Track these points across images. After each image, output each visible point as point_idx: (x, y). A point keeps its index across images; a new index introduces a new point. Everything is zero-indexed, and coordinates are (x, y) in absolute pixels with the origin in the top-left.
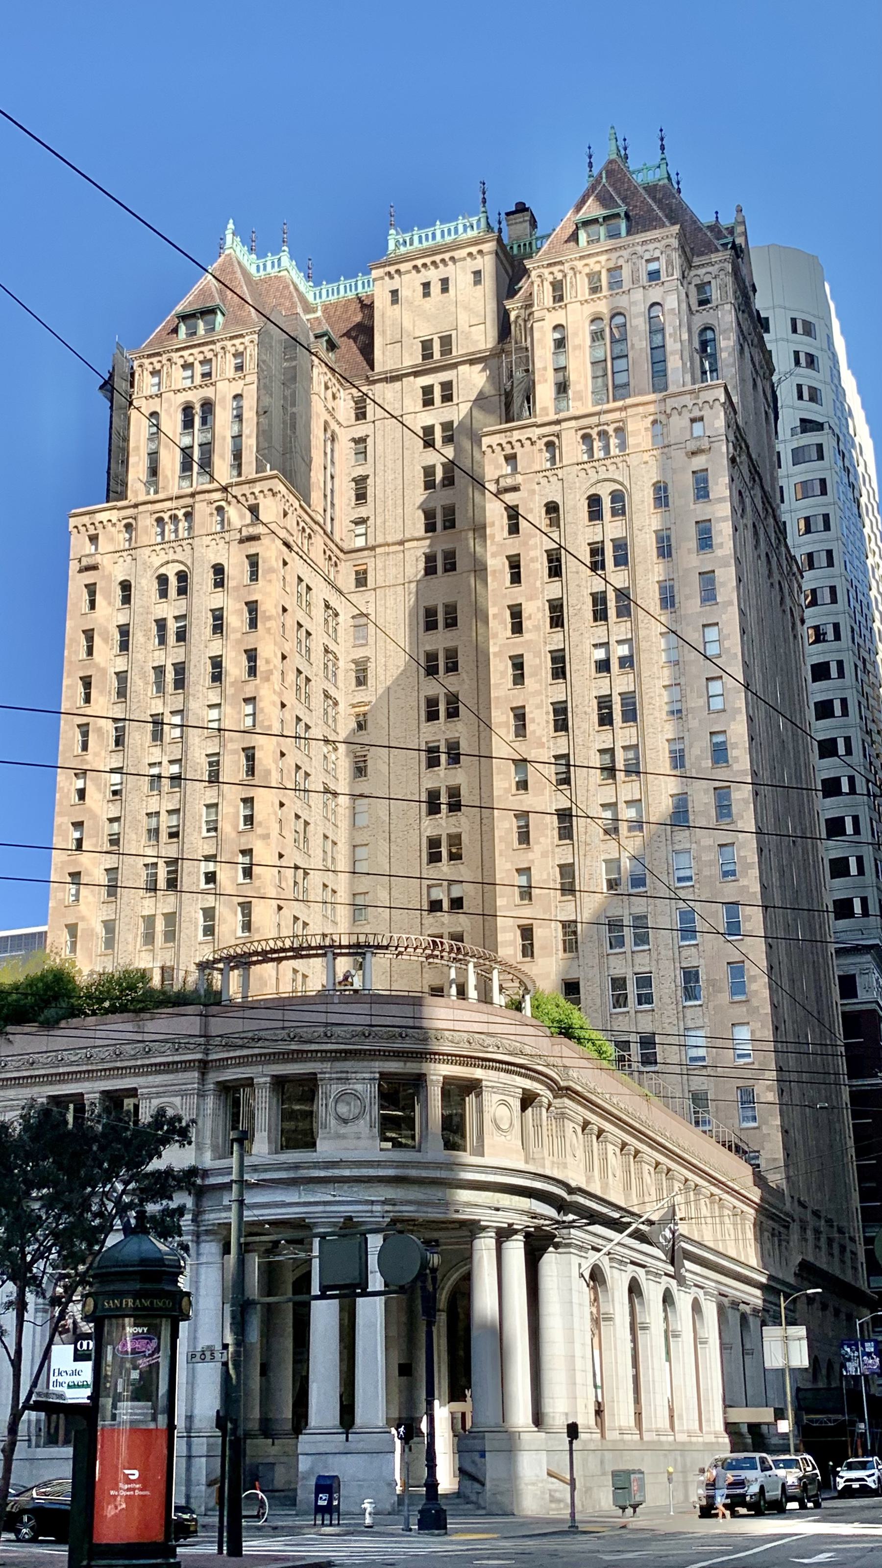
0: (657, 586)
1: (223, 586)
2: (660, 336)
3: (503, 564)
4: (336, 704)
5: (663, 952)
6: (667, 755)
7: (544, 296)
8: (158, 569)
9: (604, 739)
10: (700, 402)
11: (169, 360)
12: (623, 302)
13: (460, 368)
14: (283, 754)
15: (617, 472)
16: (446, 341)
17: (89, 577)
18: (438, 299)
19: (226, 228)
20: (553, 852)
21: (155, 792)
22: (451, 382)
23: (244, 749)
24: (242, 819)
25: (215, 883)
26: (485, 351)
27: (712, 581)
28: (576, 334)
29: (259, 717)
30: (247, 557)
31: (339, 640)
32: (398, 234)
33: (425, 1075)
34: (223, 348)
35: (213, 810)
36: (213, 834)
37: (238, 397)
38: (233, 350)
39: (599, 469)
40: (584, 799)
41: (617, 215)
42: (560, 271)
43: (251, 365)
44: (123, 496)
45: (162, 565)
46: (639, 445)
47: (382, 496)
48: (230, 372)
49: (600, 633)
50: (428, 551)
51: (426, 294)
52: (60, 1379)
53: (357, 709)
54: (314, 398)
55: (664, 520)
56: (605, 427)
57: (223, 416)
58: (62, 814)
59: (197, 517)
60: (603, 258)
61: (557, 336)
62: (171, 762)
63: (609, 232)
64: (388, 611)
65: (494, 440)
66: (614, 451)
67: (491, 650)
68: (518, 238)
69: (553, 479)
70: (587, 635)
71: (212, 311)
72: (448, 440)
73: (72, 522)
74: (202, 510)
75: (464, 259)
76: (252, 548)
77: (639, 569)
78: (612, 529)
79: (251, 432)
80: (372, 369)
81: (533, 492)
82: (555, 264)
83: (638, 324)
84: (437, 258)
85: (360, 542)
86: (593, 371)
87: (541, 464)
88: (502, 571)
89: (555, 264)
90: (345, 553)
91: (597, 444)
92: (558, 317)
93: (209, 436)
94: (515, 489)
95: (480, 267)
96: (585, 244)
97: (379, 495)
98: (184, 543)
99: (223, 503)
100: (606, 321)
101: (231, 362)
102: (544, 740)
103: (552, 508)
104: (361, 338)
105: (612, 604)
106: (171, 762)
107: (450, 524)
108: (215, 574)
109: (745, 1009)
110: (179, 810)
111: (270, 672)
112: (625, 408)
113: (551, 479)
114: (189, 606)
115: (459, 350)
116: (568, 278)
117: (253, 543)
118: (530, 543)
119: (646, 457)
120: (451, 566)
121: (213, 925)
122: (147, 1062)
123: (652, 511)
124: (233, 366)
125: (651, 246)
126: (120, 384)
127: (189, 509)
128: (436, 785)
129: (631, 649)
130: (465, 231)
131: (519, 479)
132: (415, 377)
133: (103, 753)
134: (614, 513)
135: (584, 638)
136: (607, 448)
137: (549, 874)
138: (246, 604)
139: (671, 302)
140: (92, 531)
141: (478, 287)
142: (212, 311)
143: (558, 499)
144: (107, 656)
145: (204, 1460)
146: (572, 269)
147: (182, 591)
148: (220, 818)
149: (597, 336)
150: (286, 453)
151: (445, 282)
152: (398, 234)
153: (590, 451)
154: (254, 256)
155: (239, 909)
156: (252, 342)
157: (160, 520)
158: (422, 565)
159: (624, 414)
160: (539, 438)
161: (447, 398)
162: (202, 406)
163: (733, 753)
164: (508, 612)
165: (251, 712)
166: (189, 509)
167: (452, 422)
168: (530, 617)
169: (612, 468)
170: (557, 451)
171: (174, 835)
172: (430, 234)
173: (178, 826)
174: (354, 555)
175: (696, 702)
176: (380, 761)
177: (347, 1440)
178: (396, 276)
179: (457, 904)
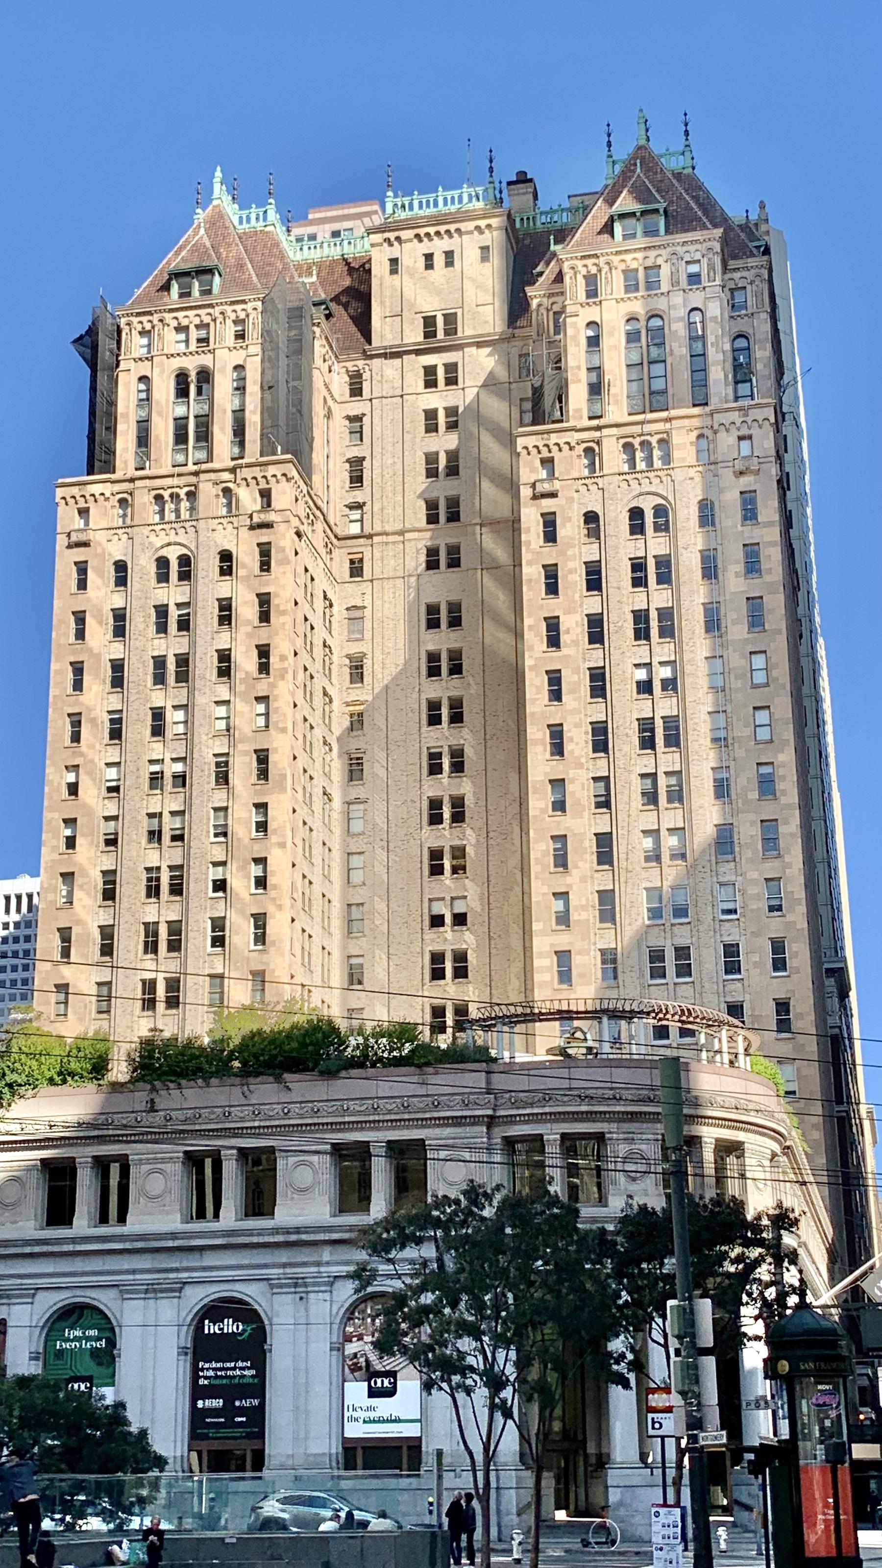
0: (701, 607)
1: (230, 574)
2: (700, 344)
3: (540, 573)
4: (331, 701)
5: (706, 985)
6: (712, 784)
7: (575, 286)
8: (157, 550)
9: (646, 763)
10: (749, 420)
11: (161, 321)
12: (661, 304)
13: (466, 350)
14: (295, 758)
15: (661, 486)
16: (450, 320)
17: (79, 554)
18: (442, 273)
19: (213, 177)
20: (592, 877)
21: (158, 791)
22: (456, 365)
23: (256, 751)
24: (254, 825)
25: (225, 891)
26: (495, 334)
27: (761, 608)
28: (611, 334)
29: (273, 718)
30: (259, 545)
31: (333, 632)
32: (396, 196)
33: (701, 1137)
34: (222, 313)
35: (222, 814)
36: (222, 839)
37: (239, 368)
38: (233, 316)
39: (642, 481)
40: (625, 824)
41: (656, 211)
42: (595, 264)
43: (254, 334)
44: (109, 467)
45: (162, 547)
46: (684, 459)
47: (379, 480)
48: (230, 340)
49: (641, 653)
50: (429, 544)
51: (429, 266)
52: (355, 1414)
53: (352, 708)
54: (316, 373)
55: (707, 540)
56: (648, 438)
57: (223, 385)
58: (51, 809)
59: (202, 497)
60: (640, 255)
61: (591, 333)
62: (174, 760)
63: (645, 227)
64: (387, 605)
65: (531, 441)
66: (657, 463)
67: (527, 663)
68: (521, 211)
69: (593, 488)
70: (628, 654)
71: (210, 271)
72: (452, 426)
73: (60, 492)
74: (208, 490)
75: (471, 232)
76: (264, 536)
77: (684, 590)
78: (655, 545)
79: (256, 407)
80: (370, 344)
81: (572, 499)
82: (589, 256)
83: (678, 329)
84: (442, 229)
85: (355, 529)
86: (628, 374)
87: (580, 471)
88: (537, 581)
89: (589, 256)
90: (339, 539)
91: (639, 455)
92: (593, 313)
93: (206, 407)
94: (553, 495)
95: (489, 243)
96: (621, 238)
97: (377, 479)
98: (187, 525)
99: (231, 485)
100: (643, 323)
101: (230, 330)
102: (583, 760)
103: (591, 518)
104: (354, 304)
105: (654, 624)
106: (174, 760)
107: (454, 517)
108: (221, 561)
109: (791, 1046)
110: (184, 811)
111: (285, 671)
112: (669, 420)
113: (590, 487)
114: (193, 593)
115: (466, 330)
116: (603, 273)
117: (264, 530)
118: (569, 553)
119: (692, 472)
120: (454, 563)
121: (224, 936)
122: (436, 1115)
123: (697, 530)
124: (233, 333)
125: (692, 248)
126: (105, 344)
127: (193, 488)
128: (439, 793)
129: (674, 671)
130: (470, 200)
131: (557, 485)
132: (417, 355)
133: (98, 746)
134: (657, 528)
135: (625, 658)
136: (649, 460)
137: (587, 899)
138: (258, 595)
139: (714, 310)
140: (82, 504)
141: (486, 264)
142: (210, 271)
143: (599, 510)
144: (99, 640)
145: (513, 1492)
146: (608, 263)
147: (185, 576)
148: (230, 822)
149: (632, 337)
150: (289, 432)
151: (449, 256)
152: (396, 196)
153: (632, 462)
154: (236, 206)
155: (252, 920)
156: (255, 309)
157: (159, 498)
158: (423, 558)
159: (668, 425)
160: (578, 444)
161: (452, 381)
162: (198, 373)
163: (780, 786)
164: (544, 625)
165: (263, 711)
166: (193, 488)
167: (457, 407)
168: (568, 631)
169: (656, 481)
170: (597, 459)
171: (178, 838)
172: (431, 200)
173: (183, 828)
174: (349, 542)
175: (742, 731)
176: (377, 765)
177: (652, 1474)
178: (396, 244)
179: (460, 919)
